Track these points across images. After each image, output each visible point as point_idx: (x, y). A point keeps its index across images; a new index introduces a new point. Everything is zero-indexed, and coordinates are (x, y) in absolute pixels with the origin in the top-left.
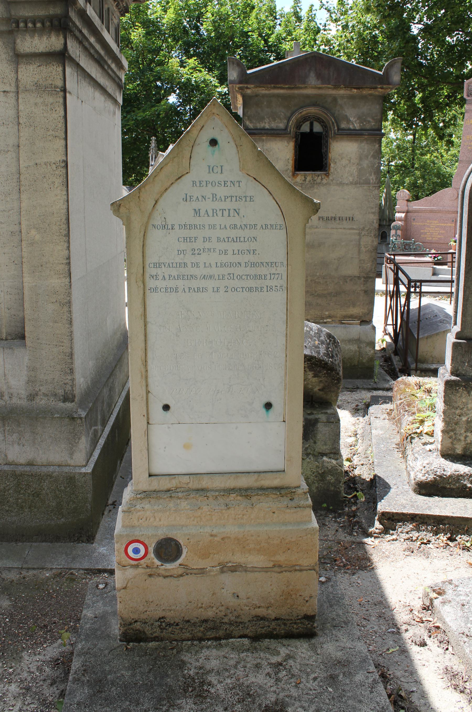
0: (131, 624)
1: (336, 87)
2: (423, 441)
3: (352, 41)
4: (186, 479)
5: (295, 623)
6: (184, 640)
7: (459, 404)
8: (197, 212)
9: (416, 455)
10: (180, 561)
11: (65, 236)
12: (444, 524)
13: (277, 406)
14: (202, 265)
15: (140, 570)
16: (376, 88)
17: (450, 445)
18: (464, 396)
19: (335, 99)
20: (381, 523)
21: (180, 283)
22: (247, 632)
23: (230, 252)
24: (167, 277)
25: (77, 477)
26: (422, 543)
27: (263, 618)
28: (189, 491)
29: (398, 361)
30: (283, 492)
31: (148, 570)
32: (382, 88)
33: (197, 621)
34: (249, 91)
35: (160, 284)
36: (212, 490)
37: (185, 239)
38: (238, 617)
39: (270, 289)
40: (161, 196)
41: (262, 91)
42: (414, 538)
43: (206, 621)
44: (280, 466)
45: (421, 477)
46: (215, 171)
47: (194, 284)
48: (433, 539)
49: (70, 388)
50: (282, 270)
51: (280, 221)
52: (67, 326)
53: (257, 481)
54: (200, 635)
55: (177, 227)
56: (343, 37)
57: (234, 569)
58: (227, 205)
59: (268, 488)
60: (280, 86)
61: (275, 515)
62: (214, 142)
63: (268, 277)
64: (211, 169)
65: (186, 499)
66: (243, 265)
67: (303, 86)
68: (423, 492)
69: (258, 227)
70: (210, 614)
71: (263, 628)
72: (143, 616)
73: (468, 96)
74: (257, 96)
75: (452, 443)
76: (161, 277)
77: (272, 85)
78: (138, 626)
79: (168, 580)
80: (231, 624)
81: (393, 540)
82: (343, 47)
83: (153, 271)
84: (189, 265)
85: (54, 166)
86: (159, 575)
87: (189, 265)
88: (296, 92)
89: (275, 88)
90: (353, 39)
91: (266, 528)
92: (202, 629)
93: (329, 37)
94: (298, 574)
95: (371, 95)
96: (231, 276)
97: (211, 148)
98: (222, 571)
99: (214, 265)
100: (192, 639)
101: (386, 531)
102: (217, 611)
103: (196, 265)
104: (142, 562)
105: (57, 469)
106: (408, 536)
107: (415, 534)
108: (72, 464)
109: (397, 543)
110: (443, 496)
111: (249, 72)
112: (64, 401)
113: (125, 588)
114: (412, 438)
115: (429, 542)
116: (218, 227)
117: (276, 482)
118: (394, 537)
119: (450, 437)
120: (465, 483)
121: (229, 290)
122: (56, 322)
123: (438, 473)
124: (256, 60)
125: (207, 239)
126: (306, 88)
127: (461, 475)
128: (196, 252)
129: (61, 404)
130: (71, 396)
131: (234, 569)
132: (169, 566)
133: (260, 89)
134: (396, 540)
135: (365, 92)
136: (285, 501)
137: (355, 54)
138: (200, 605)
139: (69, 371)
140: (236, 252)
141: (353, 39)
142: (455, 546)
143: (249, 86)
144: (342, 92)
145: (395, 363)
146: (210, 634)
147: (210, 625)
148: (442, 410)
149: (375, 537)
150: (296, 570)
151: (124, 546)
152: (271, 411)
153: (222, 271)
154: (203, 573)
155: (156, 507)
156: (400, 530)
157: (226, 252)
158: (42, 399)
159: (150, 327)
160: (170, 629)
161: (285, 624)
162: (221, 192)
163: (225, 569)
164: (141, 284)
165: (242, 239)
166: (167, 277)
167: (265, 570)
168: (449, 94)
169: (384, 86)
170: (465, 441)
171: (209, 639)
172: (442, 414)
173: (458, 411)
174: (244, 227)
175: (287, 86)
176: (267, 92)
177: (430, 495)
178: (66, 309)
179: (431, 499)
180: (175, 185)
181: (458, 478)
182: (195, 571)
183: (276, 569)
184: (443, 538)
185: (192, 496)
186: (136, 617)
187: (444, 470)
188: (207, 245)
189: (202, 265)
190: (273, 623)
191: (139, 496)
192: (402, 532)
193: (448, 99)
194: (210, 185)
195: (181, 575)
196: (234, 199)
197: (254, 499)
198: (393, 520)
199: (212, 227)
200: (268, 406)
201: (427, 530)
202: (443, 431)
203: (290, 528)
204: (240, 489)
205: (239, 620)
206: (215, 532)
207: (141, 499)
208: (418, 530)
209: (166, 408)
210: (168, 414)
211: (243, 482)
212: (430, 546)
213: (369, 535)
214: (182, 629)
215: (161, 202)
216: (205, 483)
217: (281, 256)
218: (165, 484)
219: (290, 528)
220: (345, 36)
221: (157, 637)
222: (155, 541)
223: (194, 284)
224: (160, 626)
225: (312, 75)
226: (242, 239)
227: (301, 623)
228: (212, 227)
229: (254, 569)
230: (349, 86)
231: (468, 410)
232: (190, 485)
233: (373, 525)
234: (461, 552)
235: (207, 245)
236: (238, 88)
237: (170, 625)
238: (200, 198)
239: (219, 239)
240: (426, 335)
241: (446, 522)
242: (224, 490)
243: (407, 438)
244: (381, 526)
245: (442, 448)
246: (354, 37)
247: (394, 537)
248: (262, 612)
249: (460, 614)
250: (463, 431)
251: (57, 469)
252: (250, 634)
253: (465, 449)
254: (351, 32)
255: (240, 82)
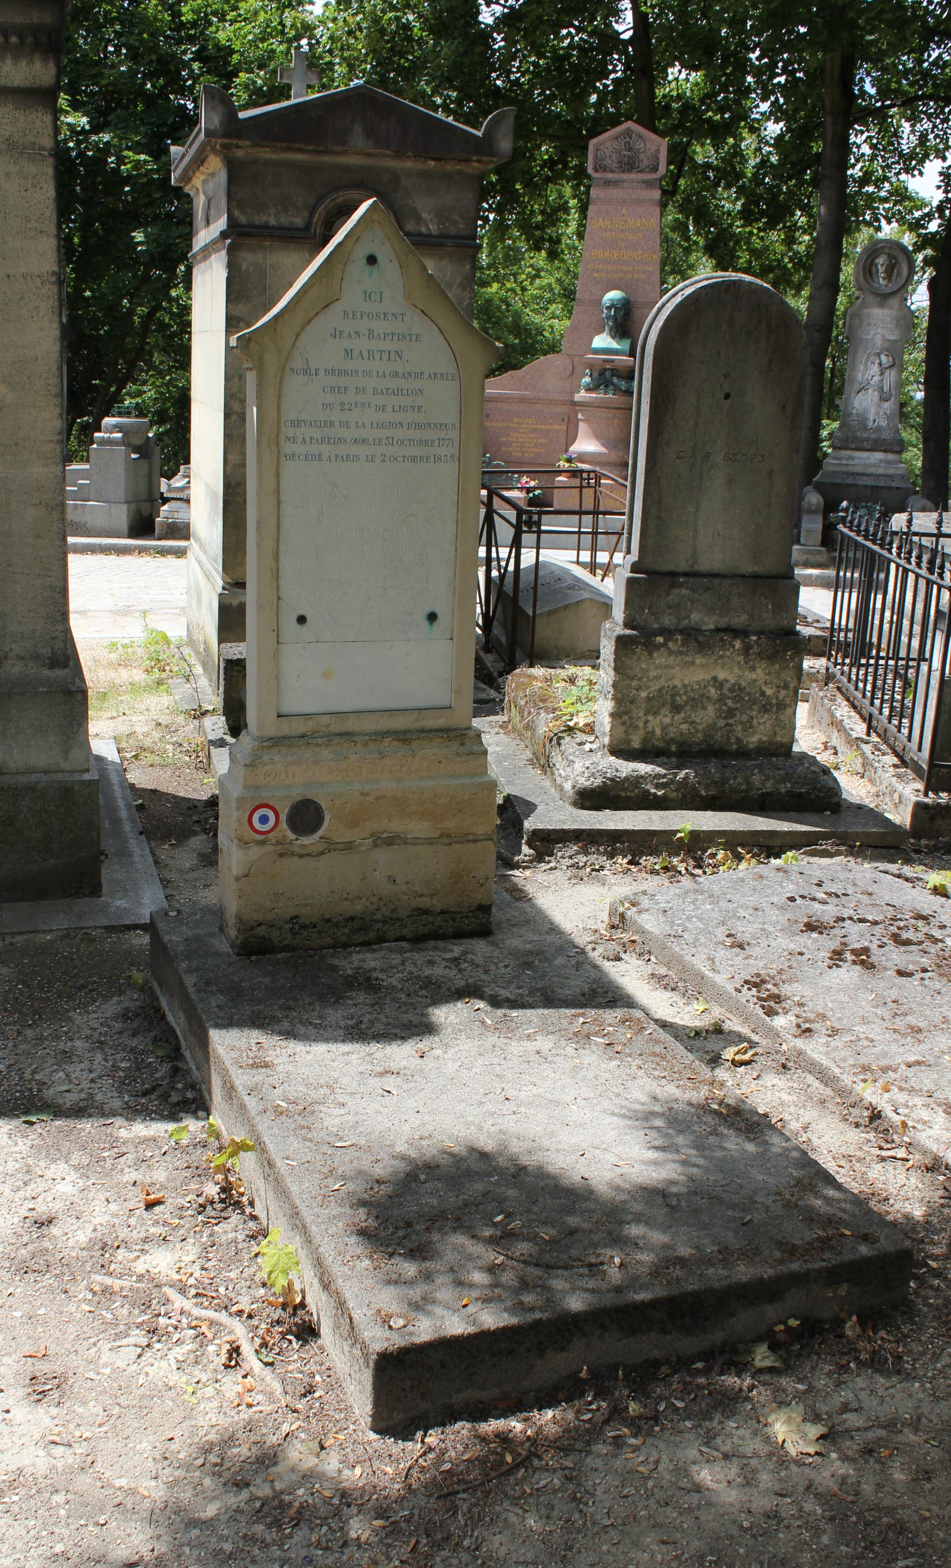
0: (252, 928)
1: (399, 154)
2: (578, 740)
3: (358, 33)
4: (325, 720)
5: (467, 917)
6: (322, 948)
7: (637, 671)
8: (348, 353)
9: (571, 758)
10: (320, 833)
11: (56, 396)
12: (622, 843)
13: (443, 617)
14: (353, 425)
15: (268, 848)
16: (469, 161)
17: (623, 735)
18: (643, 658)
19: (395, 177)
20: (531, 847)
21: (325, 449)
22: (405, 932)
23: (389, 409)
24: (308, 440)
25: (76, 788)
26: (593, 870)
27: (425, 912)
28: (330, 736)
29: (494, 661)
30: (451, 734)
31: (279, 847)
32: (479, 162)
33: (341, 918)
34: (240, 153)
35: (298, 449)
36: (359, 734)
37: (332, 389)
38: (393, 911)
39: (438, 459)
40: (303, 329)
41: (266, 154)
42: (581, 864)
43: (352, 919)
44: (445, 702)
45: (584, 782)
46: (373, 299)
47: (343, 450)
48: (607, 864)
49: (62, 645)
50: (453, 434)
51: (452, 370)
52: (58, 543)
53: (417, 720)
54: (344, 939)
55: (322, 372)
56: (341, 23)
57: (391, 841)
58: (388, 345)
59: (430, 731)
60: (297, 146)
61: (442, 766)
62: (372, 260)
63: (436, 443)
64: (368, 296)
65: (327, 746)
66: (405, 426)
67: (339, 149)
68: (588, 804)
69: (426, 376)
70: (358, 908)
71: (425, 925)
72: (270, 917)
73: (596, 170)
74: (254, 162)
75: (626, 732)
76: (299, 440)
77: (284, 145)
78: (261, 931)
79: (305, 861)
80: (384, 922)
81: (551, 869)
82: (339, 45)
83: (289, 431)
84: (337, 424)
85: (38, 281)
86: (293, 854)
87: (337, 424)
88: (327, 159)
89: (288, 149)
90: (361, 30)
91: (431, 783)
92: (347, 931)
93: (309, 19)
94: (472, 845)
95: (459, 173)
96: (390, 441)
97: (368, 268)
98: (375, 845)
99: (368, 425)
100: (334, 947)
101: (539, 858)
102: (368, 904)
103: (347, 424)
104: (271, 835)
105: (43, 777)
106: (571, 862)
107: (582, 859)
108: (68, 768)
109: (557, 873)
110: (616, 809)
111: (242, 115)
112: (51, 668)
113: (246, 876)
114: (560, 738)
115: (602, 868)
116: (375, 374)
117: (441, 722)
118: (552, 865)
119: (623, 724)
120: (648, 787)
121: (387, 459)
122: (39, 537)
123: (608, 775)
124: (154, 57)
125: (360, 390)
126: (344, 153)
127: (642, 777)
128: (347, 407)
129: (46, 672)
130: (62, 658)
131: (391, 841)
132: (306, 840)
133: (262, 150)
134: (556, 868)
135: (449, 167)
136: (454, 746)
137: (365, 61)
138: (345, 896)
139: (60, 618)
140: (397, 408)
141: (361, 30)
142: (640, 870)
143: (240, 143)
144: (409, 164)
145: (489, 665)
146: (358, 938)
147: (357, 924)
148: (611, 682)
149: (525, 868)
150: (469, 841)
151: (248, 814)
152: (436, 625)
153: (382, 433)
154: (351, 849)
155: (289, 758)
156: (559, 854)
157: (384, 409)
158: (14, 665)
159: (286, 509)
160: (305, 933)
161: (454, 919)
162: (381, 327)
163: (379, 841)
164: (274, 448)
165: (405, 392)
166: (308, 440)
167: (430, 841)
168: (551, 158)
169: (484, 159)
170: (645, 728)
171: (356, 945)
172: (611, 690)
173: (634, 683)
174: (407, 375)
175: (310, 148)
176: (273, 156)
177: (598, 808)
178: (56, 515)
179: (599, 813)
180: (321, 316)
181: (636, 781)
182: (340, 846)
183: (444, 840)
184: (622, 861)
185: (335, 741)
186: (260, 917)
187: (617, 771)
188: (361, 398)
189: (353, 425)
190: (439, 919)
191: (265, 744)
192: (563, 857)
193: (551, 169)
194: (365, 318)
195: (322, 853)
196: (396, 337)
197: (415, 744)
198: (548, 842)
199: (368, 374)
200: (432, 617)
201: (599, 853)
202: (612, 715)
203: (461, 781)
204: (396, 732)
205: (395, 915)
206: (367, 788)
207: (269, 748)
208: (586, 853)
209: (302, 620)
210: (304, 629)
211: (400, 723)
212: (606, 872)
213: (516, 866)
214: (320, 932)
215: (303, 338)
216: (351, 725)
217: (452, 416)
218: (299, 727)
219: (461, 781)
220: (345, 21)
221: (287, 946)
222: (289, 805)
223: (343, 450)
224: (291, 930)
225: (358, 129)
226: (405, 392)
227: (474, 917)
228: (368, 374)
229: (416, 841)
230: (420, 155)
231: (649, 680)
232: (331, 728)
233: (519, 852)
234: (648, 876)
235: (361, 398)
236: (221, 146)
237: (304, 927)
238: (353, 335)
239: (375, 391)
240: (547, 609)
241: (625, 839)
242: (376, 734)
243: (551, 740)
244: (532, 851)
245: (611, 741)
246: (364, 25)
247: (552, 865)
248: (425, 902)
249: (662, 919)
250: (641, 714)
251: (43, 777)
252: (409, 936)
253: (645, 741)
254: (356, 14)
255: (226, 135)
